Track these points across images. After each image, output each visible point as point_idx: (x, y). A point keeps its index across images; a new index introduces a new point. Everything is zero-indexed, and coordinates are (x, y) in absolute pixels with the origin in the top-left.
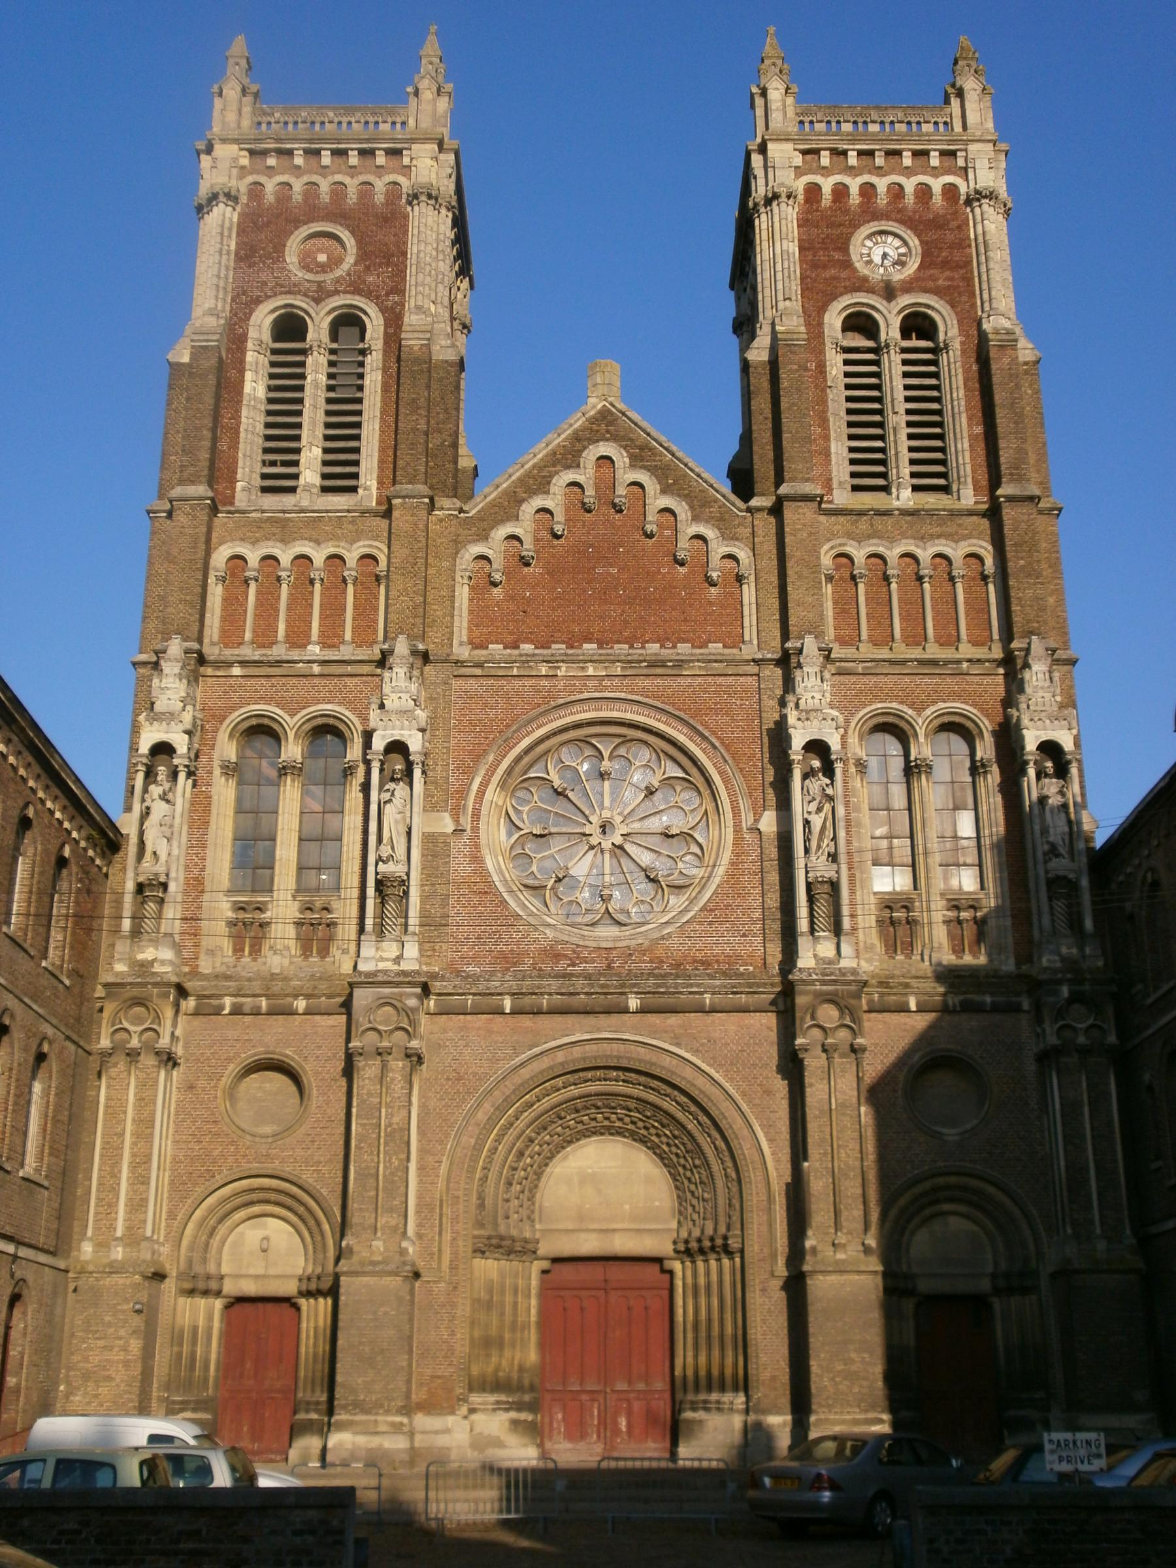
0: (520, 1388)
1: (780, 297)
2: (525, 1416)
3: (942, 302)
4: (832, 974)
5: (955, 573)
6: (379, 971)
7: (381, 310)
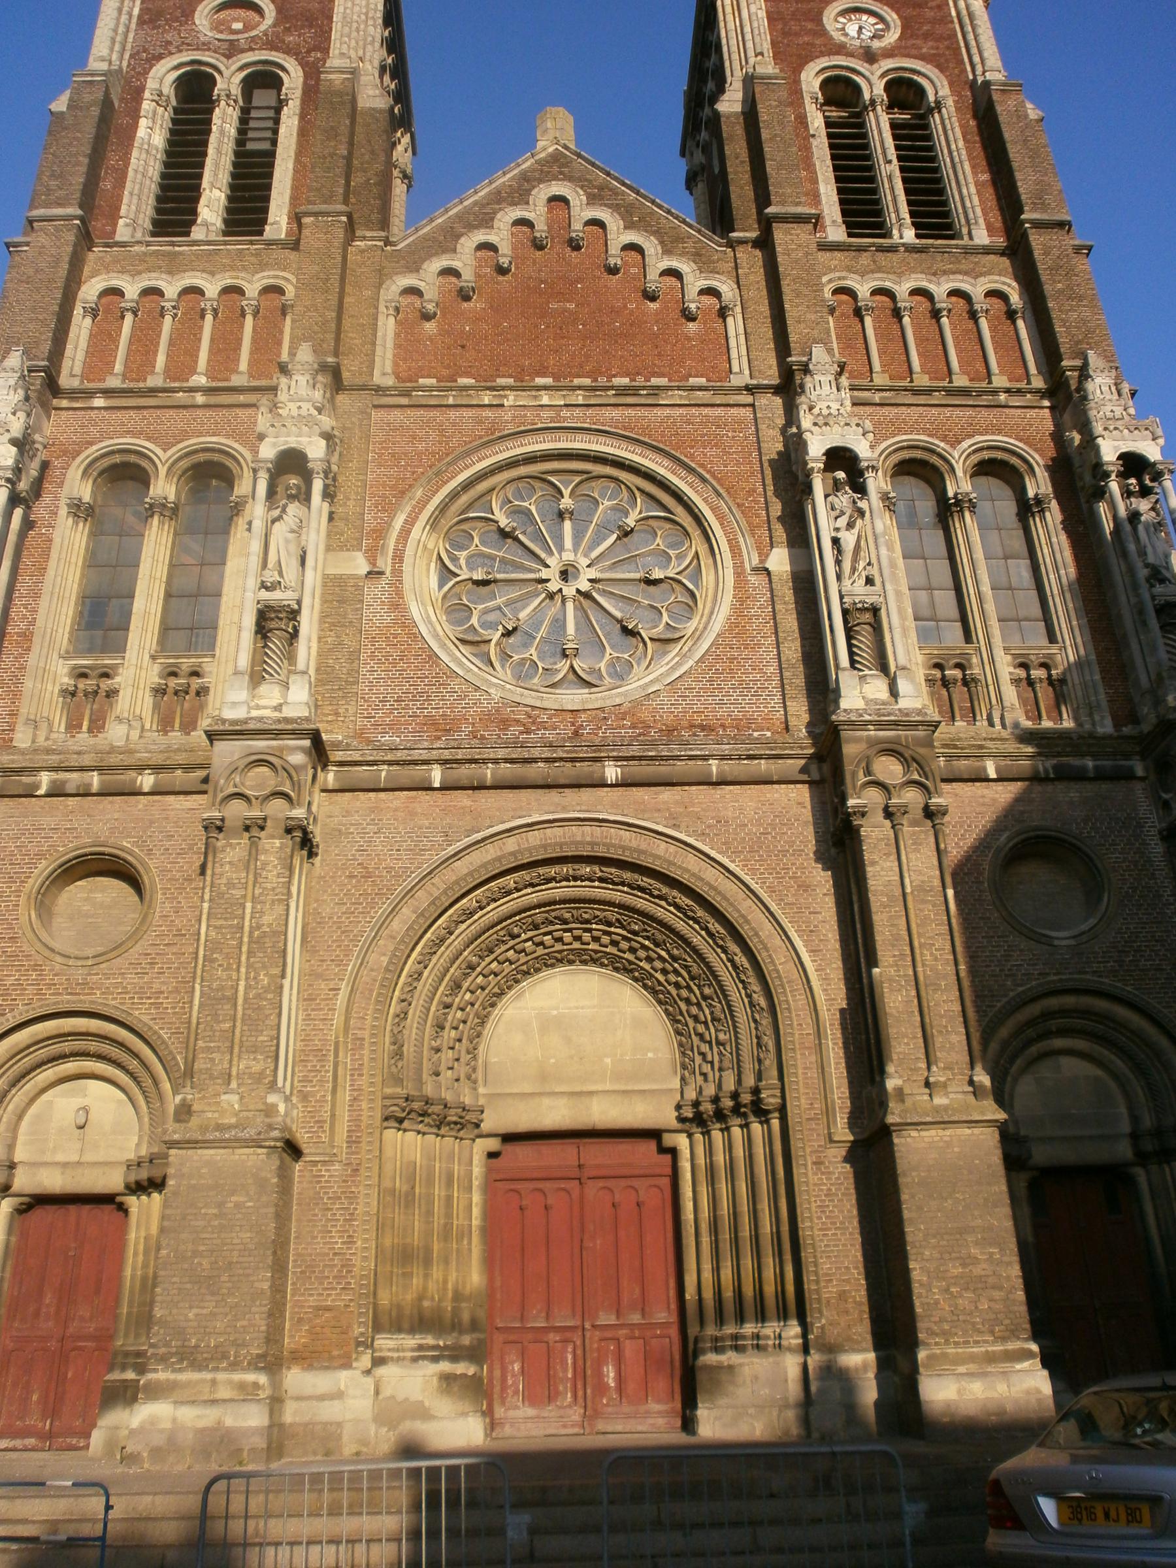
0: (455, 1326)
1: (751, 53)
2: (463, 1368)
3: (929, 66)
4: (889, 714)
5: (977, 307)
6: (251, 718)
7: (300, 64)
